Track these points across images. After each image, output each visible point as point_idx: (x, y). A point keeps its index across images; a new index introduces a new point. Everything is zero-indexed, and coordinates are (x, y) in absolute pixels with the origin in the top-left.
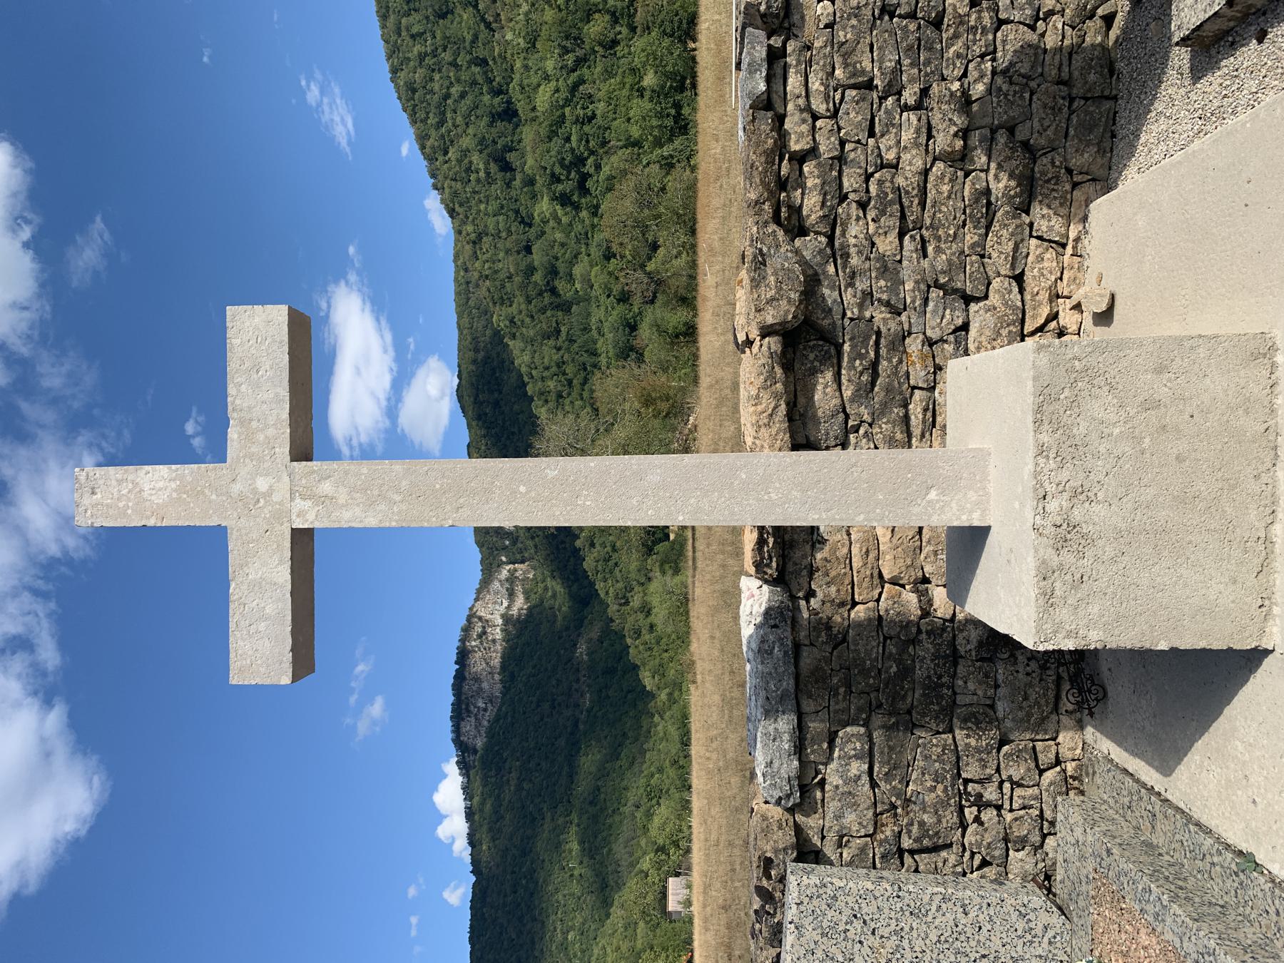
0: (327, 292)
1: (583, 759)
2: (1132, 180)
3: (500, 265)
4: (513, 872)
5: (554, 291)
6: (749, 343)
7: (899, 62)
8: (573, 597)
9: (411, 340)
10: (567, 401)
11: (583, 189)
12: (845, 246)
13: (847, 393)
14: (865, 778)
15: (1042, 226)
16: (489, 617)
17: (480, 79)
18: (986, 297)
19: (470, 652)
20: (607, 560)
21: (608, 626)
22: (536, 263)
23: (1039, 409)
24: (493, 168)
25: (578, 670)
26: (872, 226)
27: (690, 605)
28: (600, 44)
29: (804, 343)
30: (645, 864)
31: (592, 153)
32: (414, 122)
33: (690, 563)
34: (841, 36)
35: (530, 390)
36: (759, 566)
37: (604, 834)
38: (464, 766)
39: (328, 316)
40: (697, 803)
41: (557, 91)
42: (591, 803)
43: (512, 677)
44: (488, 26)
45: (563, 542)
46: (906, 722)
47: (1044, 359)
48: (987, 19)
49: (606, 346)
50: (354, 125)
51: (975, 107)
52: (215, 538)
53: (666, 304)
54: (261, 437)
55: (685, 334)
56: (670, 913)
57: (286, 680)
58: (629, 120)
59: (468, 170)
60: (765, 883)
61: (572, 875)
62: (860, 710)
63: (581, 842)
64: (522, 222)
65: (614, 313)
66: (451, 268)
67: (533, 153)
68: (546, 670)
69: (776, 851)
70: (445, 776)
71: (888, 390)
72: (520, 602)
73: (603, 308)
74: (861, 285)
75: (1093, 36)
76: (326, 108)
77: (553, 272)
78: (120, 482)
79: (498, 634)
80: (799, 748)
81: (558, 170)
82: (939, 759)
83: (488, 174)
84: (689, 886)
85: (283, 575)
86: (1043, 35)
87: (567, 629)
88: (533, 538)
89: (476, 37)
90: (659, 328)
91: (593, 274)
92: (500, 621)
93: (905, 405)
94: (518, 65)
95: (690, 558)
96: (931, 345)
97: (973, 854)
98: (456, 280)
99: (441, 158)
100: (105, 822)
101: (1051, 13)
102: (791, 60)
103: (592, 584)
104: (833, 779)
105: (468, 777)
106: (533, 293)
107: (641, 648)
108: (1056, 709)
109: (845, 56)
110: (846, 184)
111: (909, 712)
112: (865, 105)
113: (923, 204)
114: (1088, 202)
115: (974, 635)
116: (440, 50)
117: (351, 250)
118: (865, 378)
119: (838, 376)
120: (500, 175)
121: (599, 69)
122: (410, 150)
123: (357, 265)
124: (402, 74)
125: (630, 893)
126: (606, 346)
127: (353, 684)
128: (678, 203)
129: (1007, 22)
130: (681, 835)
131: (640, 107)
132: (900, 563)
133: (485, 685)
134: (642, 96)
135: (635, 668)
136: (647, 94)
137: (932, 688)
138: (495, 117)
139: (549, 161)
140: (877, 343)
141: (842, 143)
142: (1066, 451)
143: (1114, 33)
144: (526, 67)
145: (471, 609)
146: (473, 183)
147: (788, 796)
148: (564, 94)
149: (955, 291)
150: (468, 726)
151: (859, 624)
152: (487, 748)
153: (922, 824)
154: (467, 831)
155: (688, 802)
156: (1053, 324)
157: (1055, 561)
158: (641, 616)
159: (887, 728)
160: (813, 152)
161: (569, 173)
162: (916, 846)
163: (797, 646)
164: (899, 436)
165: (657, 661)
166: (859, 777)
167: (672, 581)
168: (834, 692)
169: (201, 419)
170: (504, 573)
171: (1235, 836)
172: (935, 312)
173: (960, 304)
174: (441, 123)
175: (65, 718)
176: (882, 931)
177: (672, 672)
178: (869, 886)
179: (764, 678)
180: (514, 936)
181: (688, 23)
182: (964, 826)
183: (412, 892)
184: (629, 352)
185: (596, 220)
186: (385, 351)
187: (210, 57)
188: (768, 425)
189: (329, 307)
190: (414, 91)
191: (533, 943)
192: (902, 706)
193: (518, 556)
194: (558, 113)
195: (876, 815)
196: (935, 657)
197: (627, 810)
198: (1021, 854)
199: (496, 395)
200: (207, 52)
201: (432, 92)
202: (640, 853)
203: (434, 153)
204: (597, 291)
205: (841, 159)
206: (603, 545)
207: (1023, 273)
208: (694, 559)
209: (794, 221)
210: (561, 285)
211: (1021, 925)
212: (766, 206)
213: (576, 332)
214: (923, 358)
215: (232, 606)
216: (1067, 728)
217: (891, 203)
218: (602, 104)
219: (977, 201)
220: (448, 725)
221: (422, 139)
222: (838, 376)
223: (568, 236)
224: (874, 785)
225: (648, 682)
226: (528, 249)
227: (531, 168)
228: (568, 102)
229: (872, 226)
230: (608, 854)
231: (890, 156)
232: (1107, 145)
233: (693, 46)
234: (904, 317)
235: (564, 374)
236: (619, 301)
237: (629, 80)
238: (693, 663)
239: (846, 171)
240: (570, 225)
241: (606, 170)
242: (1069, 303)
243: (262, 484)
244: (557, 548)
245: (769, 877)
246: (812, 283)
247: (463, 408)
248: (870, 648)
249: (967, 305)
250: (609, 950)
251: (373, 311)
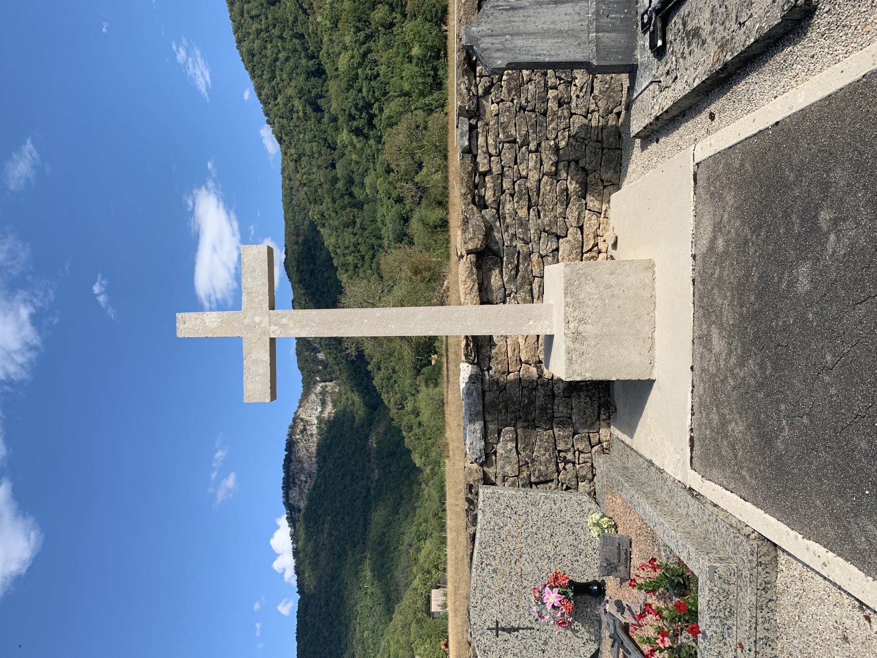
0: (192, 194)
1: (374, 514)
2: (625, 186)
3: (314, 176)
4: (326, 592)
5: (351, 195)
6: (462, 257)
7: (528, 131)
8: (366, 404)
9: (251, 227)
10: (361, 271)
11: (371, 126)
12: (504, 214)
13: (505, 279)
14: (514, 450)
15: (590, 205)
16: (308, 418)
17: (299, 48)
18: (566, 236)
19: (295, 443)
20: (389, 379)
21: (390, 424)
22: (339, 175)
23: (566, 289)
24: (309, 109)
25: (370, 454)
26: (516, 205)
27: (445, 406)
28: (382, 25)
29: (486, 257)
30: (416, 582)
31: (377, 100)
32: (253, 77)
33: (445, 379)
34: (502, 120)
35: (335, 262)
36: (466, 356)
37: (388, 565)
38: (292, 520)
39: (193, 211)
40: (450, 536)
41: (353, 57)
42: (379, 544)
43: (325, 459)
44: (305, 11)
45: (359, 367)
46: (532, 425)
47: (568, 270)
48: (566, 113)
49: (388, 232)
50: (211, 78)
51: (561, 152)
52: (237, 342)
53: (428, 206)
54: (257, 300)
55: (441, 226)
56: (433, 613)
57: (268, 400)
58: (402, 78)
59: (291, 111)
60: (470, 496)
61: (366, 593)
62: (512, 420)
63: (373, 570)
64: (329, 147)
65: (393, 210)
66: (280, 178)
67: (336, 100)
68: (348, 454)
69: (474, 481)
70: (278, 527)
71: (523, 277)
72: (329, 408)
73: (385, 207)
74: (511, 231)
75: (612, 122)
76: (190, 65)
77: (350, 181)
78: (196, 319)
79: (314, 430)
80: (485, 437)
81: (353, 111)
82: (547, 441)
83: (305, 114)
84: (445, 595)
85: (266, 357)
86: (590, 120)
87: (362, 426)
88: (338, 364)
89: (296, 20)
90: (423, 222)
91: (378, 183)
92: (316, 422)
93: (531, 285)
94: (325, 39)
95: (445, 376)
96: (542, 258)
97: (563, 484)
98: (283, 186)
99: (272, 103)
100: (39, 563)
101: (594, 111)
102: (480, 130)
103: (379, 395)
104: (500, 451)
105: (295, 528)
106: (337, 196)
107: (413, 438)
108: (599, 418)
109: (504, 128)
110: (504, 186)
111: (534, 421)
112: (513, 150)
113: (538, 195)
114: (610, 194)
115: (561, 386)
116: (271, 27)
117: (209, 165)
118: (513, 272)
119: (501, 272)
120: (313, 115)
121: (381, 42)
122: (250, 96)
123: (213, 175)
124: (244, 44)
125: (407, 601)
126: (388, 232)
127: (214, 465)
128: (435, 138)
129: (575, 114)
130: (440, 561)
131: (410, 69)
132: (529, 354)
133: (306, 465)
134: (411, 62)
135: (409, 452)
136: (415, 61)
137: (544, 410)
138: (310, 74)
139: (348, 105)
140: (518, 257)
141: (503, 167)
142: (576, 305)
143: (621, 120)
144: (331, 40)
145: (295, 413)
146: (295, 120)
147: (480, 458)
148: (357, 60)
149: (553, 233)
150: (294, 493)
151: (511, 382)
152: (308, 508)
153: (539, 470)
154: (294, 564)
155: (445, 538)
156: (596, 248)
157: (572, 347)
158: (412, 417)
159: (524, 427)
160: (490, 171)
161: (361, 114)
162: (537, 480)
163: (484, 392)
164: (528, 298)
165: (424, 447)
166: (511, 450)
167: (433, 391)
168: (500, 412)
169: (104, 282)
170: (318, 389)
171: (649, 457)
172: (543, 243)
173: (555, 239)
174: (273, 78)
175: (10, 492)
176: (518, 513)
177: (434, 454)
178: (514, 492)
179: (469, 405)
180: (327, 635)
181: (442, 13)
182: (559, 472)
183: (257, 606)
184: (403, 237)
185: (380, 146)
186: (234, 235)
187: (107, 28)
188: (470, 294)
189: (194, 204)
190: (253, 55)
191: (340, 639)
192: (530, 418)
193: (328, 377)
194: (354, 72)
195: (519, 467)
196: (545, 396)
197: (403, 548)
198: (584, 483)
199: (312, 266)
200: (105, 24)
201: (265, 56)
202: (412, 578)
203: (268, 99)
204: (381, 195)
205: (502, 175)
206: (387, 368)
207: (583, 225)
208: (448, 376)
209: (482, 202)
210: (356, 190)
211: (579, 509)
212: (469, 196)
213: (367, 223)
214: (538, 263)
215: (245, 370)
216: (604, 427)
217: (524, 194)
218: (384, 66)
219: (562, 193)
220: (281, 492)
221: (259, 89)
222: (501, 272)
223: (361, 156)
224: (518, 453)
225: (418, 461)
226: (333, 166)
227: (335, 109)
228: (360, 65)
229: (516, 205)
230: (391, 578)
231: (524, 173)
232: (618, 169)
233: (446, 28)
234: (530, 245)
235: (359, 251)
236: (396, 202)
237: (402, 50)
238: (447, 444)
239: (504, 180)
240: (362, 149)
241: (387, 112)
242: (602, 239)
243: (257, 319)
244: (355, 371)
245: (471, 493)
246: (489, 230)
247: (288, 275)
248: (516, 392)
249: (558, 240)
250: (392, 643)
251: (225, 207)
